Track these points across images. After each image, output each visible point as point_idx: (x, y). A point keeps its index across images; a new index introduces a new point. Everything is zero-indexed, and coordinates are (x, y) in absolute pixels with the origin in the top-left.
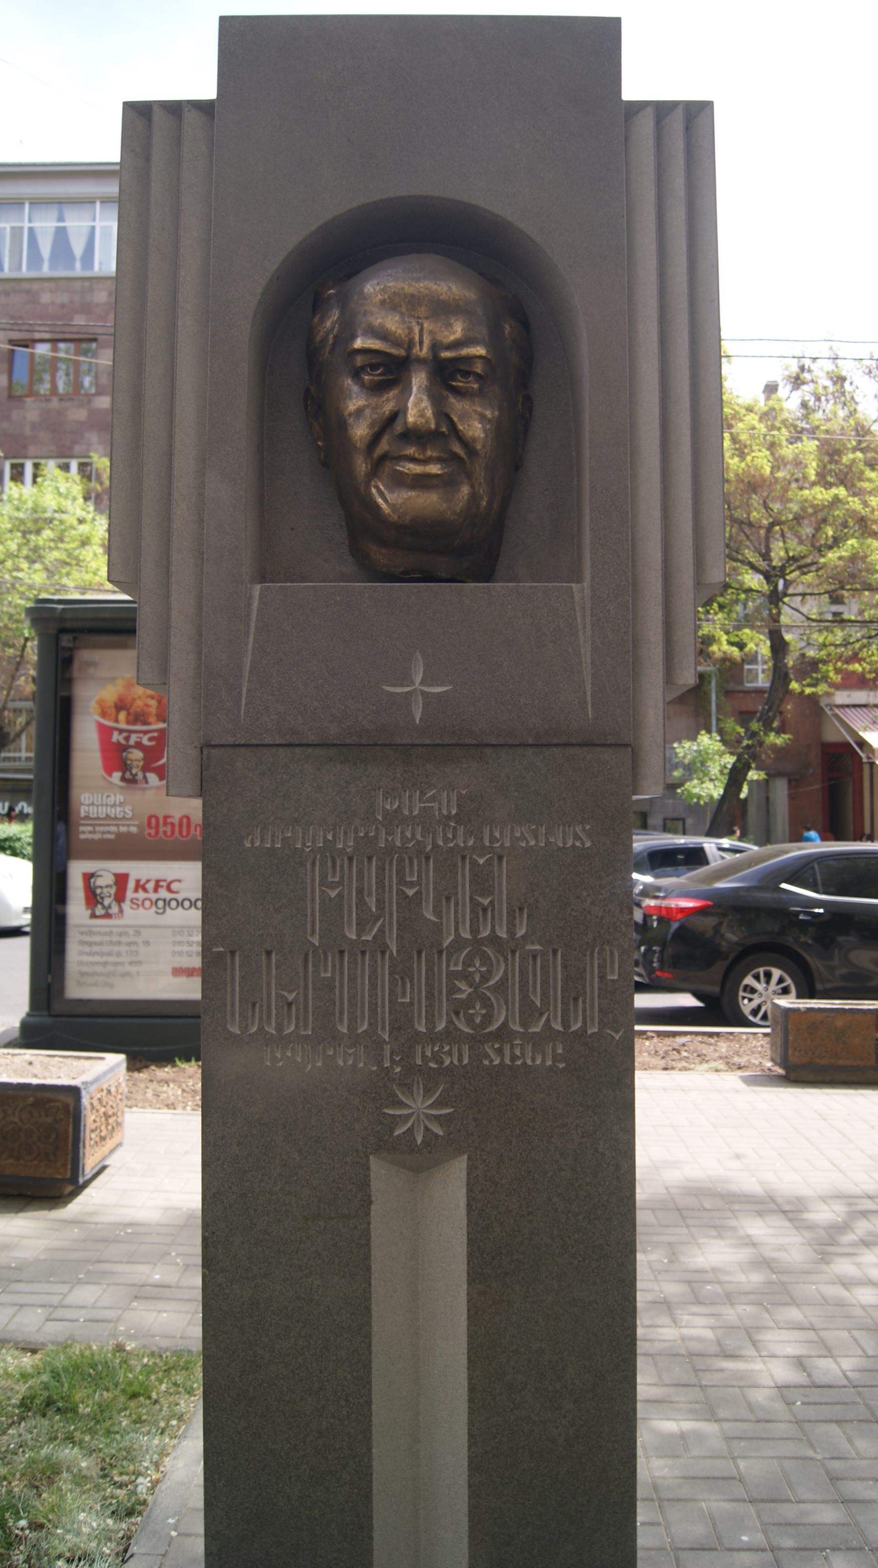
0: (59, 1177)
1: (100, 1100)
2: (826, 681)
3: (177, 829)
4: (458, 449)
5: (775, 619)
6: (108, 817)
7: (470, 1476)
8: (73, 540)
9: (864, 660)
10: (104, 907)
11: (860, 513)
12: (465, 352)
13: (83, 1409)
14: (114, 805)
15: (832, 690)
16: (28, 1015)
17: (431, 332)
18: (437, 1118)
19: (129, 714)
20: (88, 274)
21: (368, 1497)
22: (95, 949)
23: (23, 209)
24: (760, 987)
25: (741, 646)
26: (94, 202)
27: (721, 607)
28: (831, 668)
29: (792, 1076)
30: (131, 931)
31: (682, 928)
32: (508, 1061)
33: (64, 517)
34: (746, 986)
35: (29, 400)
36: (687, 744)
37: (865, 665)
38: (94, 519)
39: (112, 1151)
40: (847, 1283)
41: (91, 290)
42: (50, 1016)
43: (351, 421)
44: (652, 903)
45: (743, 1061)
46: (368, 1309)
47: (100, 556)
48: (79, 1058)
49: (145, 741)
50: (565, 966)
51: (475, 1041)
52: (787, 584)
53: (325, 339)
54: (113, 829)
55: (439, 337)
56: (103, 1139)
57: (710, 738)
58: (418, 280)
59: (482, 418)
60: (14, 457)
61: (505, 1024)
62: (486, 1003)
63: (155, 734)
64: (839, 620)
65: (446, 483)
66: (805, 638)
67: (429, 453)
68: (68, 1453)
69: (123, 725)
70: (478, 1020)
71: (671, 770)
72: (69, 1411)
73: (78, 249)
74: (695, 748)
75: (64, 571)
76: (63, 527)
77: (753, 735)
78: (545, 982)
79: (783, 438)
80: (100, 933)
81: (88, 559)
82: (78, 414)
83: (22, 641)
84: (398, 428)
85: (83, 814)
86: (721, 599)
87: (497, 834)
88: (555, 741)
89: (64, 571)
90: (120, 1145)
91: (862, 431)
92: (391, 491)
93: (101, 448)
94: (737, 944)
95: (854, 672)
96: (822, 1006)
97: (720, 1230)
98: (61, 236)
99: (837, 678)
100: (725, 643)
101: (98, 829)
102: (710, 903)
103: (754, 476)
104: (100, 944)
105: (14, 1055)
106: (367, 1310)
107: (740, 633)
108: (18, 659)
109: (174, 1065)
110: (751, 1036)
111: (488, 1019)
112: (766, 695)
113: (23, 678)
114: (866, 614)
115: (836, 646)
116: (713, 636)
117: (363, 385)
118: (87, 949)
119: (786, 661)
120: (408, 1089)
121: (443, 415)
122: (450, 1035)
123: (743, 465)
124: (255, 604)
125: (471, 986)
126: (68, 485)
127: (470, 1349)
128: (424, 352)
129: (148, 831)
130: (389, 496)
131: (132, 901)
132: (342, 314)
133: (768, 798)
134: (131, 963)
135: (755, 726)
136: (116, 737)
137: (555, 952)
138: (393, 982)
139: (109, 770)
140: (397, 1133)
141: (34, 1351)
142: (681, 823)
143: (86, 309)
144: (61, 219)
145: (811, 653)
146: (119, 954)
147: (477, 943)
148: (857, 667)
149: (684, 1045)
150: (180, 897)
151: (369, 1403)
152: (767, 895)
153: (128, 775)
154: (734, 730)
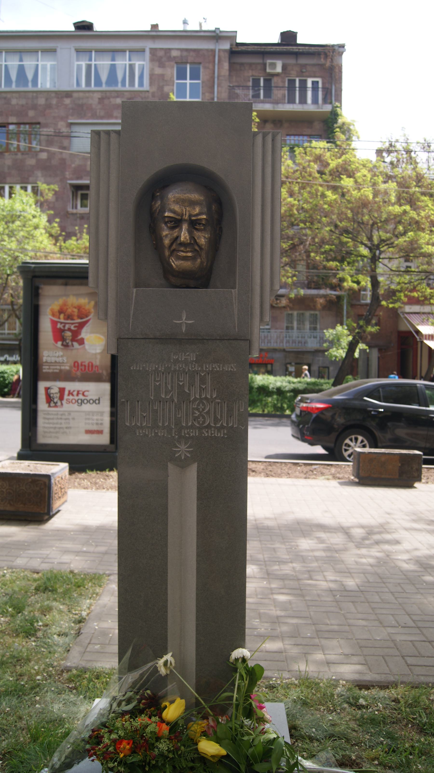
0: (42, 512)
1: (58, 481)
2: (400, 301)
3: (87, 368)
4: (197, 248)
5: (374, 270)
6: (56, 362)
7: (197, 558)
8: (30, 226)
9: (419, 291)
10: (54, 403)
11: (415, 219)
12: (199, 217)
13: (60, 590)
14: (58, 357)
15: (402, 305)
16: (21, 450)
17: (189, 211)
18: (188, 451)
19: (65, 315)
20: (35, 89)
21: (166, 564)
22: (51, 421)
23: (2, 55)
24: (352, 444)
25: (358, 283)
26: (38, 52)
28: (402, 294)
30: (66, 413)
31: (317, 417)
32: (210, 435)
33: (26, 214)
35: (6, 154)
36: (331, 331)
37: (419, 293)
38: (40, 216)
39: (63, 503)
41: (37, 98)
42: (31, 450)
43: (164, 238)
44: (305, 405)
45: (341, 476)
49: (72, 328)
50: (227, 407)
51: (200, 429)
52: (381, 253)
53: (156, 210)
54: (58, 367)
55: (191, 213)
56: (60, 497)
57: (343, 328)
58: (185, 194)
59: (205, 237)
61: (209, 424)
63: (77, 325)
64: (407, 271)
65: (193, 259)
66: (390, 279)
67: (188, 249)
68: (55, 604)
69: (62, 320)
70: (201, 422)
71: (323, 343)
72: (54, 591)
73: (30, 76)
74: (334, 333)
75: (26, 242)
76: (25, 220)
77: (360, 327)
78: (221, 411)
79: (380, 181)
80: (52, 414)
81: (38, 236)
82: (31, 162)
83: (6, 276)
84: (179, 242)
85: (44, 360)
86: (348, 260)
87: (208, 366)
88: (226, 338)
89: (26, 242)
90: (66, 501)
91: (419, 178)
92: (176, 261)
93: (42, 179)
95: (414, 297)
96: (375, 451)
98: (21, 70)
99: (406, 300)
100: (350, 281)
101: (51, 367)
102: (330, 405)
103: (364, 200)
104: (53, 419)
105: (21, 463)
106: (167, 508)
107: (357, 277)
108: (4, 285)
109: (86, 472)
110: (347, 466)
111: (204, 422)
112: (368, 308)
113: (6, 295)
114: (420, 268)
115: (405, 284)
117: (167, 227)
118: (47, 421)
119: (378, 291)
121: (192, 237)
122: (193, 427)
123: (359, 194)
124: (134, 295)
125: (199, 412)
126: (28, 198)
127: (197, 520)
128: (186, 217)
129: (74, 368)
130: (175, 263)
131: (67, 400)
132: (161, 203)
134: (67, 428)
135: (361, 323)
136: (59, 326)
137: (225, 402)
138: (175, 410)
139: (56, 341)
140: (176, 455)
141: (38, 573)
142: (327, 370)
143: (34, 107)
144: (21, 60)
145: (393, 287)
146: (61, 424)
147: (201, 399)
148: (415, 294)
149: (315, 469)
150: (88, 398)
151: (167, 536)
152: (356, 402)
153: (65, 343)
154: (351, 325)
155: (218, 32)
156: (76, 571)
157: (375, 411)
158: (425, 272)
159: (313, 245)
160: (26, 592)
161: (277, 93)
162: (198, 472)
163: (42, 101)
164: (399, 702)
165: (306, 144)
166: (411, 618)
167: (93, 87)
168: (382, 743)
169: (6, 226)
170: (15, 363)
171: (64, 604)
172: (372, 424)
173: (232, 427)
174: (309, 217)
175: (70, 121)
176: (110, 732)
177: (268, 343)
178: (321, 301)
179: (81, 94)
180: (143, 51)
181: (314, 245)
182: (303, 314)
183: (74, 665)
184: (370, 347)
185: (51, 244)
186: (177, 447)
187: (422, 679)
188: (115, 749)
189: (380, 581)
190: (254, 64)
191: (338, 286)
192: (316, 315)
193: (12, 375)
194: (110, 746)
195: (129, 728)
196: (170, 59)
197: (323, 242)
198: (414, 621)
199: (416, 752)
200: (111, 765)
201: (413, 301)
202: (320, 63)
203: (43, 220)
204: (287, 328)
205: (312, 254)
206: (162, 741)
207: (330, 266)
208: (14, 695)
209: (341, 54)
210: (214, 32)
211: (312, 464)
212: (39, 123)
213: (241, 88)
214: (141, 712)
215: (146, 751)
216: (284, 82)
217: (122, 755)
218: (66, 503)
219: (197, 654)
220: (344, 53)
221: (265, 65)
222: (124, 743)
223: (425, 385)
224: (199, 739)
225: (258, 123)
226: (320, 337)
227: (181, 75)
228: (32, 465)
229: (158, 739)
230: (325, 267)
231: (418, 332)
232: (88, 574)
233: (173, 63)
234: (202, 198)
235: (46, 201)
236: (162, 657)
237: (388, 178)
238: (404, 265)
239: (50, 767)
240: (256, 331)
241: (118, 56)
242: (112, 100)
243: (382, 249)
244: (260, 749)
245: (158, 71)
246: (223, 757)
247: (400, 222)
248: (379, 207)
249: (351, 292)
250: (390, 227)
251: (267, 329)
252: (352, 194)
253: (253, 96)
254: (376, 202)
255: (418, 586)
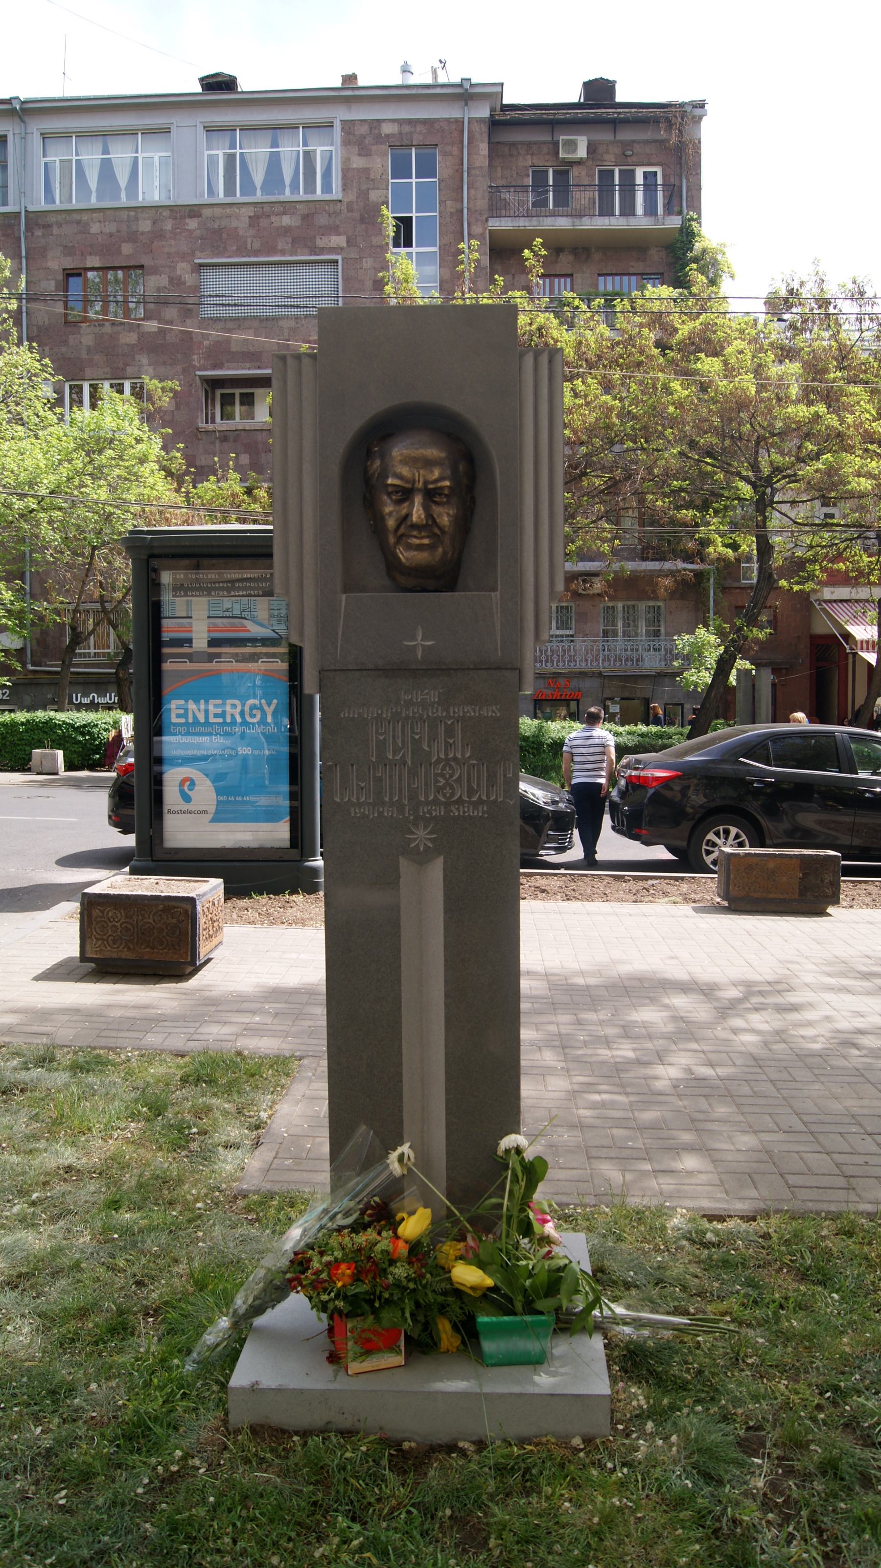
4: (437, 531)
21: (400, 1008)
25: (735, 546)
27: (716, 512)
28: (817, 567)
29: (733, 907)
34: (709, 841)
40: (735, 1031)
41: (137, 219)
45: (697, 897)
46: (399, 925)
47: (156, 472)
48: (190, 881)
51: (447, 805)
52: (774, 491)
56: (211, 936)
59: (448, 514)
60: (73, 380)
62: (452, 787)
65: (431, 547)
67: (423, 534)
68: (214, 1101)
71: (672, 660)
78: (479, 778)
84: (409, 523)
86: (716, 505)
90: (221, 943)
93: (151, 370)
94: (701, 806)
95: (838, 571)
97: (653, 1000)
109: (251, 897)
111: (452, 795)
115: (823, 547)
116: (709, 539)
117: (391, 499)
120: (416, 825)
121: (429, 515)
122: (435, 802)
124: (343, 604)
133: (754, 685)
138: (409, 778)
141: (183, 1056)
143: (133, 237)
144: (106, 151)
145: (799, 553)
147: (447, 760)
151: (400, 967)
155: (467, 85)
156: (246, 1053)
157: (759, 782)
158: (857, 525)
159: (650, 481)
160: (167, 1085)
161: (581, 198)
162: (445, 870)
163: (145, 226)
164: (771, 1238)
165: (635, 293)
166: (801, 1119)
167: (238, 198)
168: (738, 1292)
169: (87, 459)
170: (109, 708)
171: (230, 1102)
172: (753, 806)
173: (495, 801)
174: (640, 430)
175: (197, 261)
176: (322, 1254)
177: (569, 661)
178: (667, 582)
179: (218, 211)
180: (330, 126)
181: (652, 480)
182: (634, 606)
183: (253, 1188)
184: (758, 666)
185: (169, 490)
186: (413, 833)
187: (810, 1205)
188: (329, 1275)
189: (753, 1063)
190: (535, 143)
191: (700, 555)
192: (659, 607)
193: (106, 730)
194: (322, 1272)
195: (350, 1246)
196: (379, 139)
197: (667, 474)
198: (805, 1123)
199: (791, 1306)
200: (325, 1297)
201: (837, 579)
202: (659, 138)
203: (154, 447)
204: (606, 633)
205: (650, 497)
206: (398, 1264)
207: (682, 518)
208: (163, 1230)
209: (698, 120)
210: (460, 86)
211: (647, 878)
212: (141, 267)
213: (512, 190)
214: (366, 1227)
215: (374, 1278)
216: (593, 176)
217: (340, 1284)
218: (221, 947)
219: (448, 1145)
220: (704, 118)
221: (556, 144)
222: (343, 1267)
223: (849, 733)
224: (451, 1264)
225: (544, 257)
226: (666, 650)
227: (401, 170)
228: (161, 882)
229: (392, 1262)
230: (673, 521)
231: (848, 636)
232: (267, 1056)
233: (385, 147)
234: (443, 455)
235: (159, 410)
236: (395, 1150)
237: (786, 353)
238: (820, 511)
239: (231, 1314)
240: (529, 655)
241: (284, 137)
242: (273, 218)
243: (778, 485)
244: (543, 1277)
245: (358, 162)
246: (490, 1289)
247: (807, 436)
248: (770, 410)
249: (722, 563)
250: (791, 444)
251: (567, 636)
252: (718, 386)
253: (534, 205)
254: (762, 401)
255: (816, 1072)
